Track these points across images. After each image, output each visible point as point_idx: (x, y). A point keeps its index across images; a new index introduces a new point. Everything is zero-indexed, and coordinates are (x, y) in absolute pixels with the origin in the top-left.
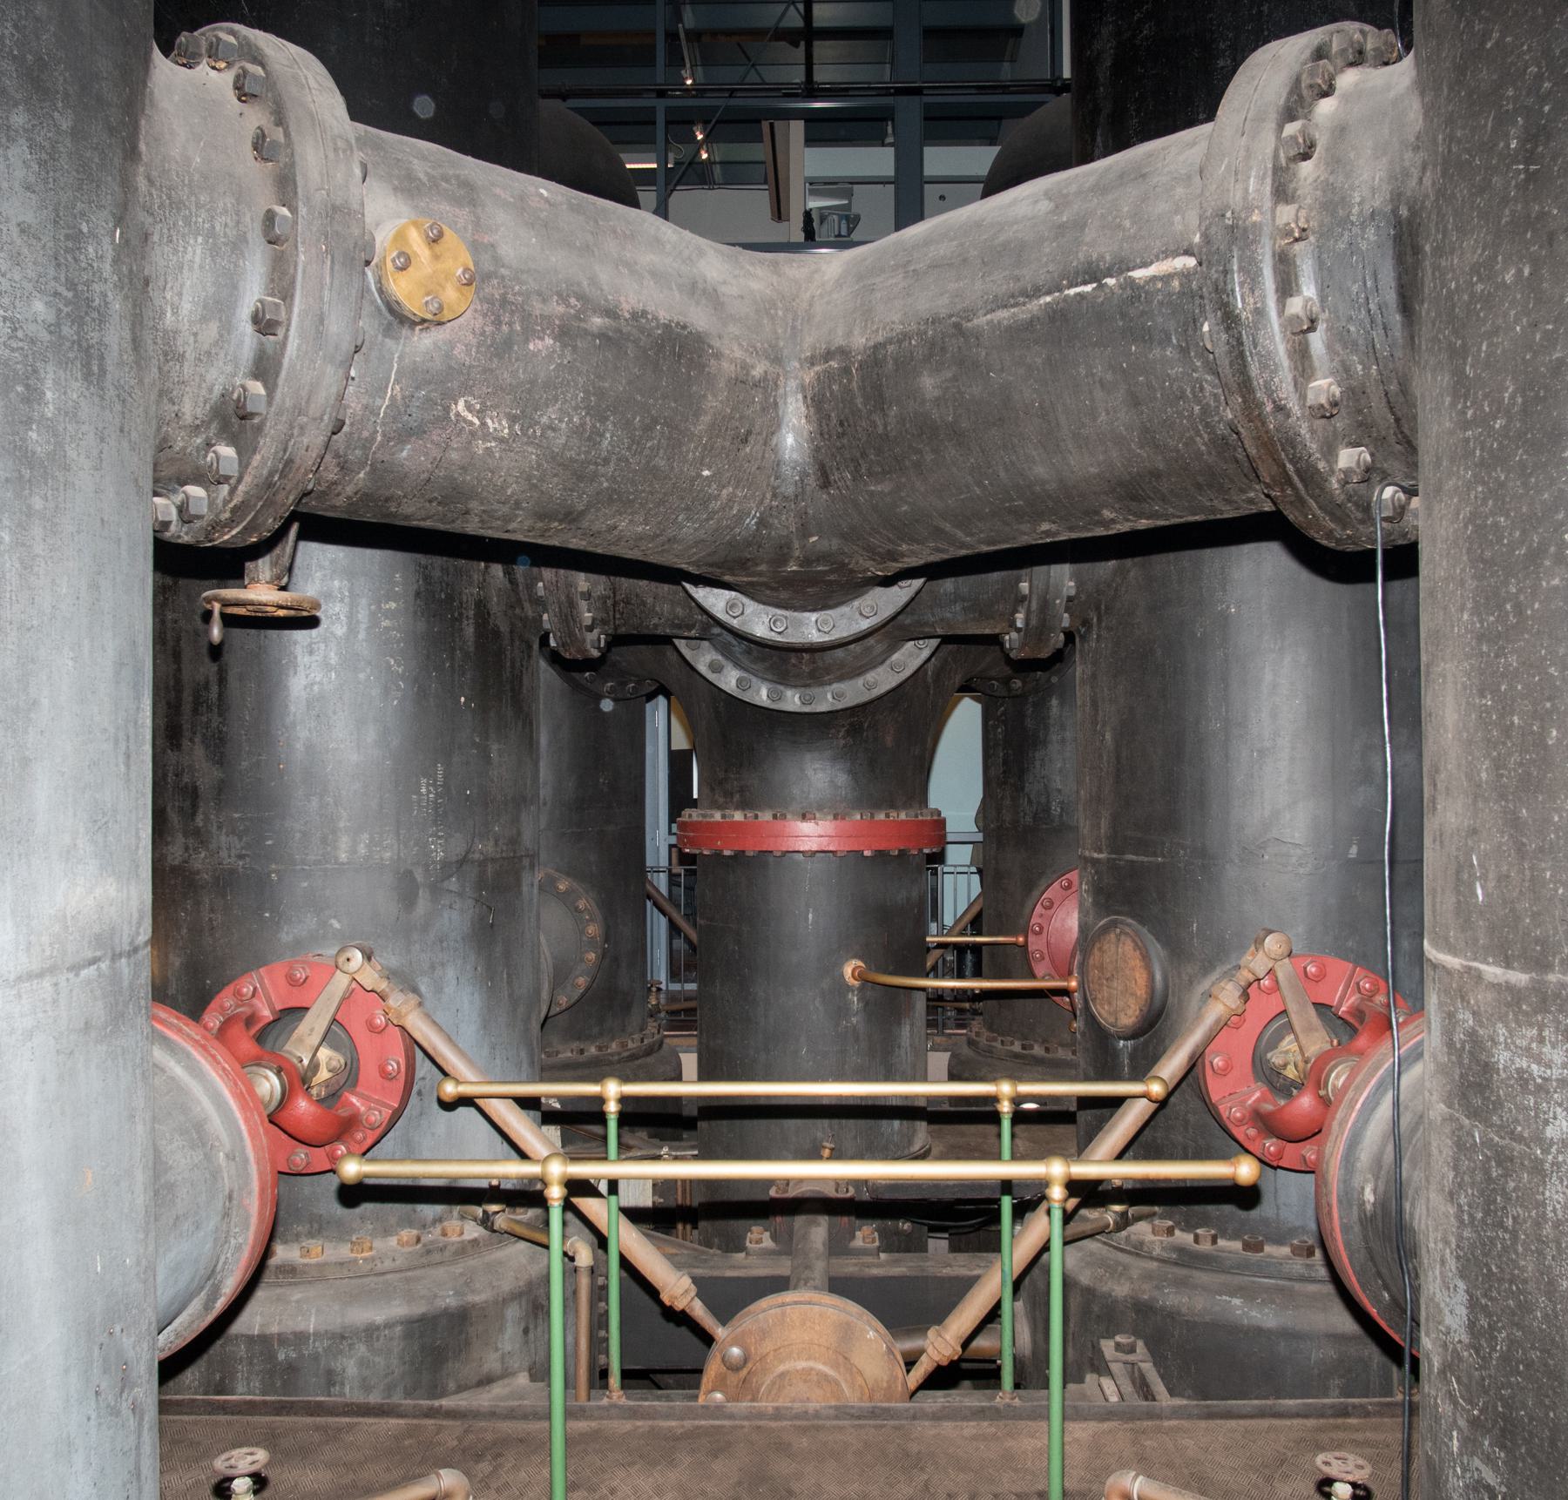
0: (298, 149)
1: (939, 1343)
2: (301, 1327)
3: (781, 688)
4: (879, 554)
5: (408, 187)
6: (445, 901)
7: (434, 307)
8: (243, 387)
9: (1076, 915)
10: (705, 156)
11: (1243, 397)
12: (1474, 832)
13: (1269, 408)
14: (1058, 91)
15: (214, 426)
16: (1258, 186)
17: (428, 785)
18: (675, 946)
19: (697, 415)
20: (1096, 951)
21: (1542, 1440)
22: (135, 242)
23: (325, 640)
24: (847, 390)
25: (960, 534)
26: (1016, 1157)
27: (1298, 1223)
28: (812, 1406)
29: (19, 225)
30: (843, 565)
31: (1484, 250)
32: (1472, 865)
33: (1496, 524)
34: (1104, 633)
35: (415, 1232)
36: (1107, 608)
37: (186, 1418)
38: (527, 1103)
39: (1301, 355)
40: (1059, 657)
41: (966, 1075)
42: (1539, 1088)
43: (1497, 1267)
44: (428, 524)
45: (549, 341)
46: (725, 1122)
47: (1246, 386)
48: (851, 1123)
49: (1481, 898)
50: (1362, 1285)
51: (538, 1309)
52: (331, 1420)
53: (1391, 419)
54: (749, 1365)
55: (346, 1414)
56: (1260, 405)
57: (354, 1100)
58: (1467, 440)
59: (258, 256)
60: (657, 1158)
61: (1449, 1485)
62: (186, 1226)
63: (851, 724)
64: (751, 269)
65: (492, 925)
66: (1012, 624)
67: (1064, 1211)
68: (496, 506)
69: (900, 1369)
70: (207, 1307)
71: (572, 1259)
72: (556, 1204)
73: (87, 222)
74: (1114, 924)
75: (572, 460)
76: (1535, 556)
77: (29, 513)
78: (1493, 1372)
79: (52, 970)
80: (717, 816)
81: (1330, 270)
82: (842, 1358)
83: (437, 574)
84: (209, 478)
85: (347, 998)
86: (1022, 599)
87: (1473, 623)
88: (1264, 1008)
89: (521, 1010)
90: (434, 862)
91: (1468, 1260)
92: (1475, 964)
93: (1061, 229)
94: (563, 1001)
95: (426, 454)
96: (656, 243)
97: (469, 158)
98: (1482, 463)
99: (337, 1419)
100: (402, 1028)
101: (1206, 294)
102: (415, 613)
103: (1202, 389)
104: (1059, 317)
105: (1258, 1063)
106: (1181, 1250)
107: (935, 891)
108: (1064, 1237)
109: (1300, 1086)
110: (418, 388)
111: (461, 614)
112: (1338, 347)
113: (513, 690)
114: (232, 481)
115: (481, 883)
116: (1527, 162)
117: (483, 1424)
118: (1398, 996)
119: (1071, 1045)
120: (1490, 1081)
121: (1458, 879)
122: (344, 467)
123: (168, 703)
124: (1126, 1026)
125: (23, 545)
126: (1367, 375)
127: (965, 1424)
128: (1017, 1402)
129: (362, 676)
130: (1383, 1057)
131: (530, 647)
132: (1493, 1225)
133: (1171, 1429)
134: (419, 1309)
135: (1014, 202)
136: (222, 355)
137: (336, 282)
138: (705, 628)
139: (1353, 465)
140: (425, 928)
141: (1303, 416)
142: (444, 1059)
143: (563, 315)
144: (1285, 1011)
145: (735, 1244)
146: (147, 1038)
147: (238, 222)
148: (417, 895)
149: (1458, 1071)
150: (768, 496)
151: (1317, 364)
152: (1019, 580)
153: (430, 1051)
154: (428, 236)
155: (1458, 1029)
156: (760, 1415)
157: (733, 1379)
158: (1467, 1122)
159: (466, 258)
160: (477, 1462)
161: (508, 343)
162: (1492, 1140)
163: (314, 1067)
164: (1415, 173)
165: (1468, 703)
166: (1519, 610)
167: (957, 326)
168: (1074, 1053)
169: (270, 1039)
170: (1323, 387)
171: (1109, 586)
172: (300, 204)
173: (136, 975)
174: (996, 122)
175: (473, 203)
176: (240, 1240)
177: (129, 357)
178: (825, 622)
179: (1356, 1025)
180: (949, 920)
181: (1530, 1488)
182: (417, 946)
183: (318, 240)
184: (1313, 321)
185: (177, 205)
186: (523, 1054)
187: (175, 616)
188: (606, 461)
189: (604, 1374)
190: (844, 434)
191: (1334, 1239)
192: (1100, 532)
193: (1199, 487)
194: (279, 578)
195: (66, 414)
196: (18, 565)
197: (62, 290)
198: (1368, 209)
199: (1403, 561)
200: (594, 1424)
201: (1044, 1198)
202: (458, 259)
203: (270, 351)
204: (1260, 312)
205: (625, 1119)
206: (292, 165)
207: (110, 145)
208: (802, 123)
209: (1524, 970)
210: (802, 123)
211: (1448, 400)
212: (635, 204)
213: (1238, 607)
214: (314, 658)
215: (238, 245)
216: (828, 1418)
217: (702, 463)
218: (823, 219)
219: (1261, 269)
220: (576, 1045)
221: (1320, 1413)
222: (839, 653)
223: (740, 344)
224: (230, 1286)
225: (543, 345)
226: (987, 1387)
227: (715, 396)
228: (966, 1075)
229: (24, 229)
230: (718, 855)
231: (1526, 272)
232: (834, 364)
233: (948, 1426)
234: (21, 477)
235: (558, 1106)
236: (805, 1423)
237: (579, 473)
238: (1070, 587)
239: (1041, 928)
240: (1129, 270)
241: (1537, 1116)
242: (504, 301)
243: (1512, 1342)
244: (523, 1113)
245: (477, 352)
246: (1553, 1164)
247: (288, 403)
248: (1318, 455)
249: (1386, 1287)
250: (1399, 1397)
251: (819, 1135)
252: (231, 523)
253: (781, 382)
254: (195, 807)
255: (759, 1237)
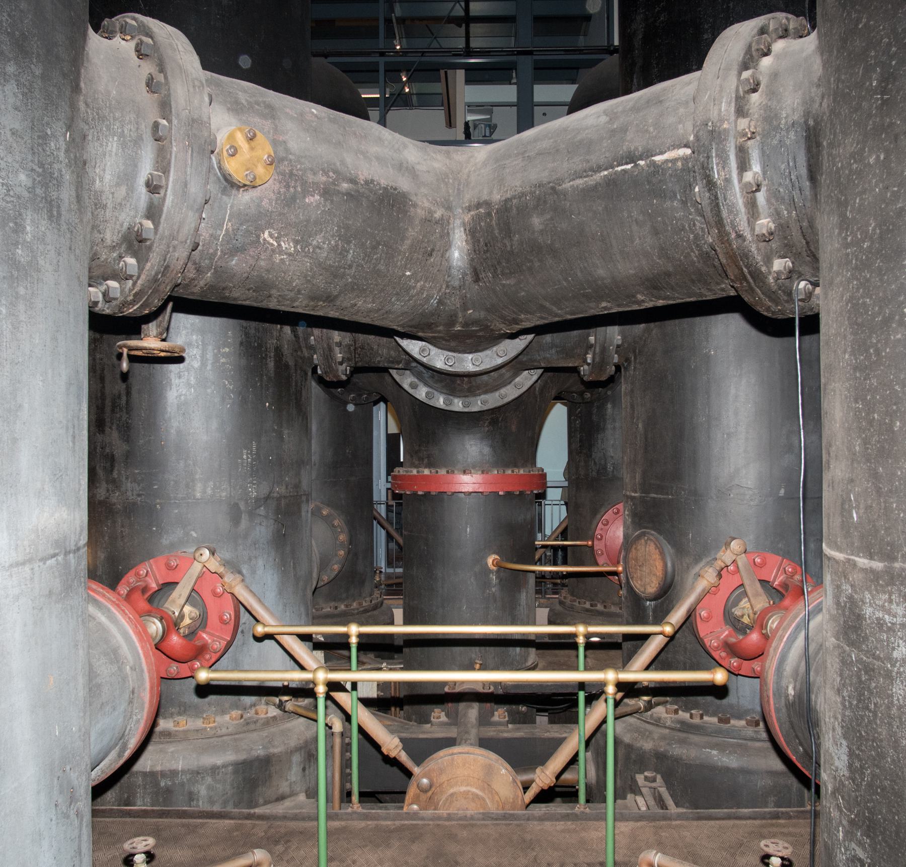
0: (172, 86)
1: (542, 776)
2: (174, 767)
3: (451, 397)
4: (508, 320)
5: (236, 108)
6: (257, 521)
7: (251, 177)
8: (140, 223)
9: (622, 529)
10: (407, 90)
11: (718, 229)
12: (852, 481)
13: (733, 236)
14: (611, 53)
15: (124, 246)
16: (727, 108)
17: (247, 454)
18: (390, 547)
19: (403, 240)
20: (633, 550)
21: (891, 832)
22: (78, 140)
23: (188, 370)
24: (489, 225)
25: (554, 309)
26: (587, 669)
27: (750, 707)
28: (469, 813)
29: (11, 130)
30: (487, 327)
31: (857, 145)
32: (850, 500)
33: (864, 303)
34: (638, 366)
35: (240, 712)
36: (640, 351)
37: (107, 820)
38: (305, 638)
39: (752, 205)
40: (612, 380)
41: (558, 621)
42: (889, 629)
43: (865, 732)
44: (247, 303)
45: (317, 197)
46: (419, 649)
47: (720, 223)
48: (492, 649)
49: (855, 519)
50: (787, 743)
51: (311, 757)
52: (191, 821)
53: (804, 242)
54: (433, 789)
55: (200, 817)
56: (728, 234)
57: (205, 636)
58: (848, 255)
59: (149, 148)
60: (380, 669)
61: (837, 859)
62: (108, 708)
63: (492, 419)
64: (434, 155)
65: (284, 535)
66: (585, 361)
67: (615, 700)
68: (286, 293)
69: (520, 792)
70: (120, 755)
71: (331, 728)
72: (321, 696)
73: (51, 128)
74: (644, 534)
75: (330, 266)
76: (887, 321)
77: (17, 296)
78: (862, 793)
79: (30, 561)
80: (415, 472)
81: (768, 156)
82: (486, 785)
83: (252, 332)
84: (121, 276)
85: (200, 577)
86: (590, 346)
87: (851, 360)
88: (730, 583)
89: (301, 584)
90: (251, 498)
91: (848, 728)
92: (852, 557)
93: (613, 132)
94: (326, 578)
95: (246, 263)
96: (379, 141)
97: (271, 92)
98: (856, 268)
99: (195, 820)
100: (232, 594)
101: (697, 170)
102: (240, 354)
103: (694, 225)
104: (612, 183)
105: (727, 614)
106: (683, 723)
107: (540, 515)
108: (615, 715)
109: (751, 628)
110: (241, 224)
111: (266, 355)
112: (773, 201)
113: (296, 399)
114: (134, 278)
115: (278, 511)
116: (883, 94)
117: (279, 823)
118: (808, 576)
119: (619, 604)
120: (861, 625)
121: (842, 508)
122: (199, 270)
123: (97, 407)
124: (650, 593)
125: (13, 315)
126: (790, 217)
127: (558, 823)
128: (588, 810)
129: (209, 391)
130: (799, 611)
131: (306, 374)
132: (863, 708)
133: (677, 826)
134: (242, 756)
135: (586, 117)
136: (128, 205)
137: (194, 163)
138: (408, 363)
139: (782, 269)
140: (246, 537)
141: (753, 240)
142: (257, 612)
143: (325, 182)
144: (742, 584)
145: (424, 719)
146: (85, 600)
147: (138, 129)
148: (241, 517)
149: (842, 619)
150: (444, 287)
151: (761, 210)
152: (589, 335)
153: (249, 607)
154: (247, 137)
155: (842, 595)
156: (439, 818)
157: (424, 797)
158: (848, 648)
159: (269, 149)
160: (276, 845)
161: (293, 198)
162: (862, 659)
163: (182, 616)
164: (818, 100)
165: (848, 406)
166: (878, 352)
167: (553, 188)
168: (621, 608)
169: (156, 601)
170: (765, 223)
171: (641, 339)
172: (173, 118)
173: (79, 564)
174: (575, 71)
175: (273, 117)
176: (139, 717)
177: (74, 207)
178: (477, 360)
179: (784, 592)
180: (548, 532)
181: (884, 860)
182: (241, 547)
183: (184, 139)
184: (758, 186)
185: (102, 119)
186: (302, 609)
187: (101, 356)
188: (350, 267)
189: (349, 794)
190: (487, 251)
191: (771, 716)
192: (636, 307)
193: (693, 281)
194: (161, 334)
195: (38, 239)
196: (10, 327)
197: (36, 167)
198: (790, 121)
199: (811, 324)
200: (343, 823)
201: (603, 692)
202: (265, 150)
203: (156, 203)
204: (728, 181)
205: (361, 647)
206: (169, 95)
207: (64, 84)
208: (463, 71)
209: (880, 561)
210: (463, 71)
211: (837, 231)
212: (367, 118)
213: (715, 351)
214: (182, 380)
215: (138, 141)
216: (478, 819)
217: (406, 268)
218: (475, 127)
219: (729, 156)
220: (333, 604)
221: (763, 817)
222: (485, 378)
223: (427, 199)
224: (133, 743)
225: (314, 199)
226: (570, 802)
227: (413, 229)
228: (558, 621)
229: (14, 133)
230: (415, 494)
231: (882, 157)
232: (482, 210)
233: (548, 824)
234: (12, 276)
235: (322, 639)
236: (465, 822)
237: (335, 274)
238: (618, 339)
239: (602, 536)
240: (652, 156)
241: (888, 645)
242: (291, 174)
243: (873, 776)
244: (302, 643)
245: (276, 204)
246: (897, 673)
247: (167, 233)
248: (762, 263)
249: (801, 744)
250: (809, 808)
251: (473, 656)
252: (133, 302)
253: (451, 221)
254: (112, 466)
255: (439, 715)
